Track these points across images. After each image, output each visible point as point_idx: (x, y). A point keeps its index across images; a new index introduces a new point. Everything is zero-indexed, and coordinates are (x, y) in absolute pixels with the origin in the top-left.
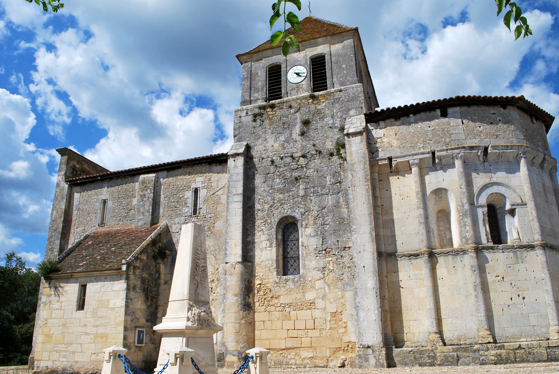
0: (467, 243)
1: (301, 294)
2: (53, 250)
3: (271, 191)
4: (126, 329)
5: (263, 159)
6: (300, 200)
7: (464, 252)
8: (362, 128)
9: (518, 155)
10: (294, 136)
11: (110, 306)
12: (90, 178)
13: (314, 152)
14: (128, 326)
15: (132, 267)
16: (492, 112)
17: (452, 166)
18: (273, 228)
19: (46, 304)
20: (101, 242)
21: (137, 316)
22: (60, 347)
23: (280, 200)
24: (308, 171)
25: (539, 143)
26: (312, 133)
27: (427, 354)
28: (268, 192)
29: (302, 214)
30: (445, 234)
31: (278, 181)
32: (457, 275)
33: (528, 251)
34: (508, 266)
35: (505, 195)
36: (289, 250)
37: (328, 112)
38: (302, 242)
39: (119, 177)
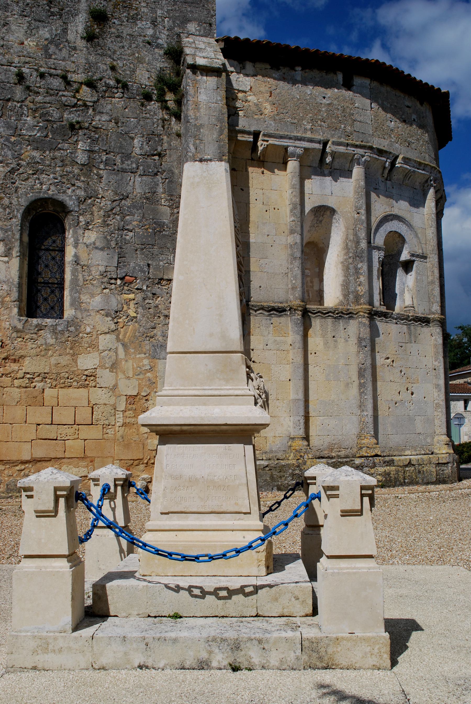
3: (13, 139)
6: (76, 171)
9: (427, 181)
13: (112, 83)
16: (407, 103)
17: (348, 174)
18: (16, 217)
23: (33, 163)
24: (97, 118)
26: (109, 42)
27: (290, 471)
28: (7, 140)
29: (81, 201)
30: (312, 282)
33: (422, 327)
34: (401, 345)
35: (405, 237)
36: (40, 268)
37: (146, 10)
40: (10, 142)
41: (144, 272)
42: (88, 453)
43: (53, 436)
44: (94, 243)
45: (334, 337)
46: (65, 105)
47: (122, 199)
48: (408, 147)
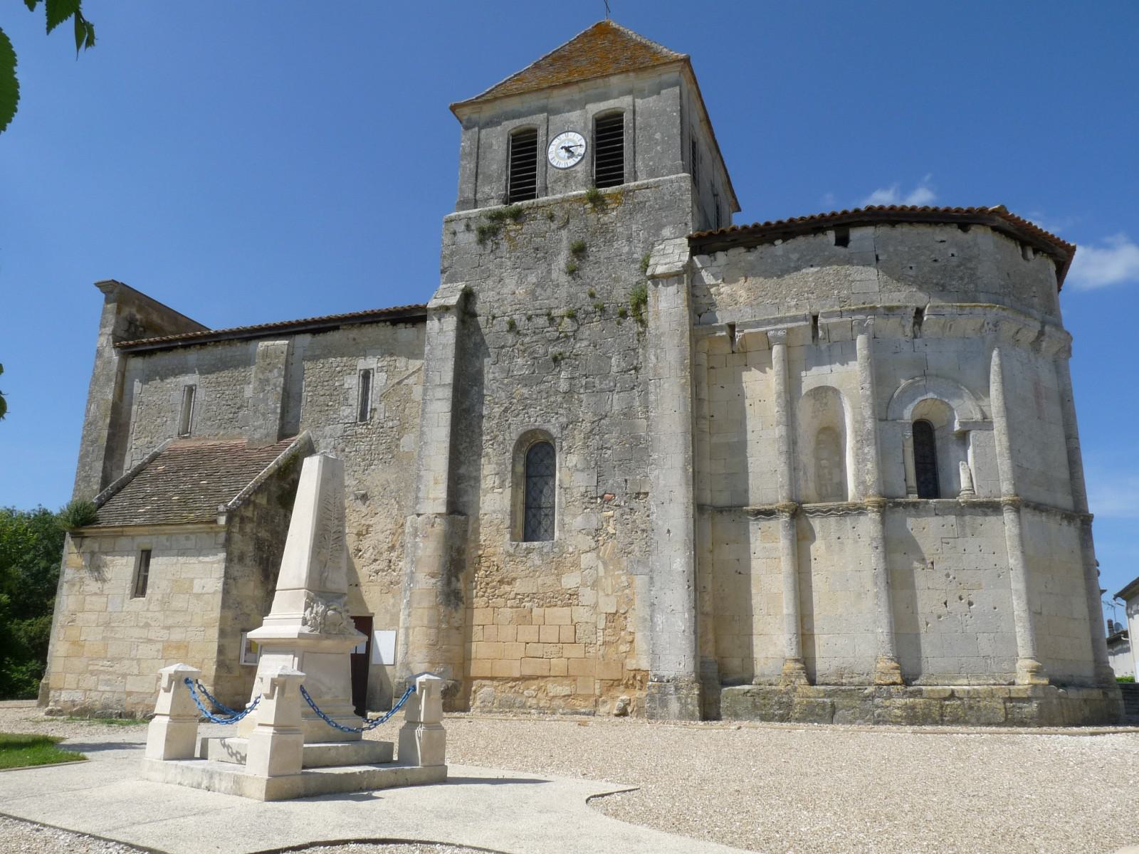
0: (865, 495)
1: (554, 577)
2: (90, 481)
3: (506, 381)
4: (222, 633)
5: (494, 318)
6: (559, 399)
7: (859, 510)
8: (680, 264)
10: (554, 276)
11: (195, 591)
12: (164, 342)
13: (590, 309)
14: (229, 629)
15: (237, 519)
16: (939, 238)
18: (508, 451)
19: (74, 585)
20: (181, 469)
21: (247, 610)
22: (101, 665)
23: (523, 399)
24: (578, 345)
25: (1036, 300)
26: (588, 271)
29: (563, 428)
30: (830, 474)
31: (520, 361)
32: (847, 558)
38: (560, 480)
39: (219, 341)
40: (503, 384)
41: (622, 488)
42: (571, 673)
43: (540, 654)
44: (576, 466)
45: (839, 538)
46: (549, 341)
47: (600, 419)
48: (942, 291)
